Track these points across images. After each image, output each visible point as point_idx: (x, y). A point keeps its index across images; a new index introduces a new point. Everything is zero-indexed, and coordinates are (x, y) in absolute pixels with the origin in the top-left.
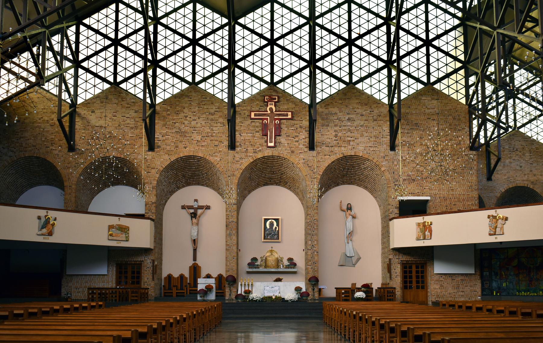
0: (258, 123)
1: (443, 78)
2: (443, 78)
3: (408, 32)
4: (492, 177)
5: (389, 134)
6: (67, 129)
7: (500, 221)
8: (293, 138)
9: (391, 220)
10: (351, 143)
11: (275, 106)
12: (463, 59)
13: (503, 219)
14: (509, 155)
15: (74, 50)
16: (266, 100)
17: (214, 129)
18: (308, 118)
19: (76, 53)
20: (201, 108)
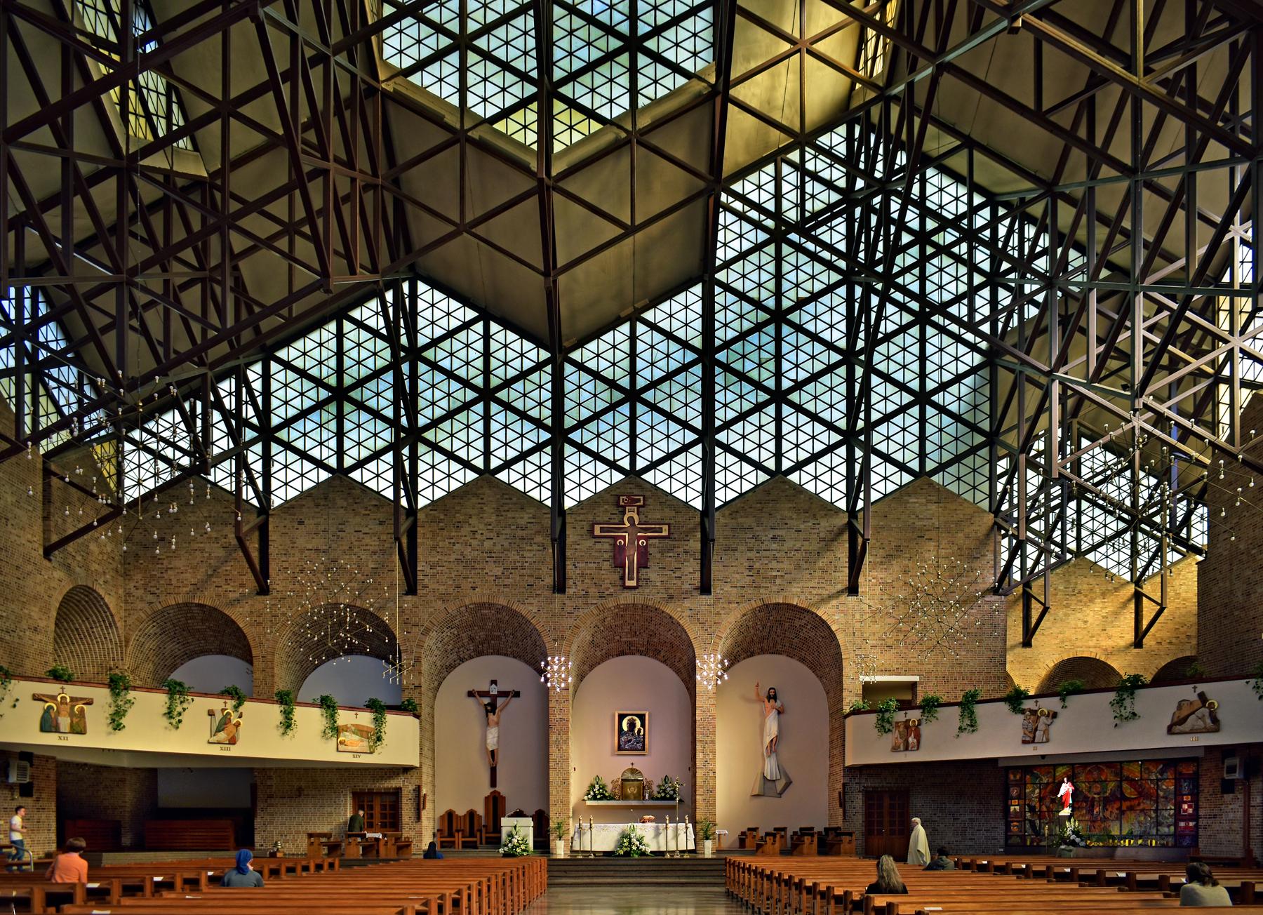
10: (778, 581)
11: (638, 514)
13: (1048, 716)
16: (622, 503)
17: (526, 554)
19: (264, 413)
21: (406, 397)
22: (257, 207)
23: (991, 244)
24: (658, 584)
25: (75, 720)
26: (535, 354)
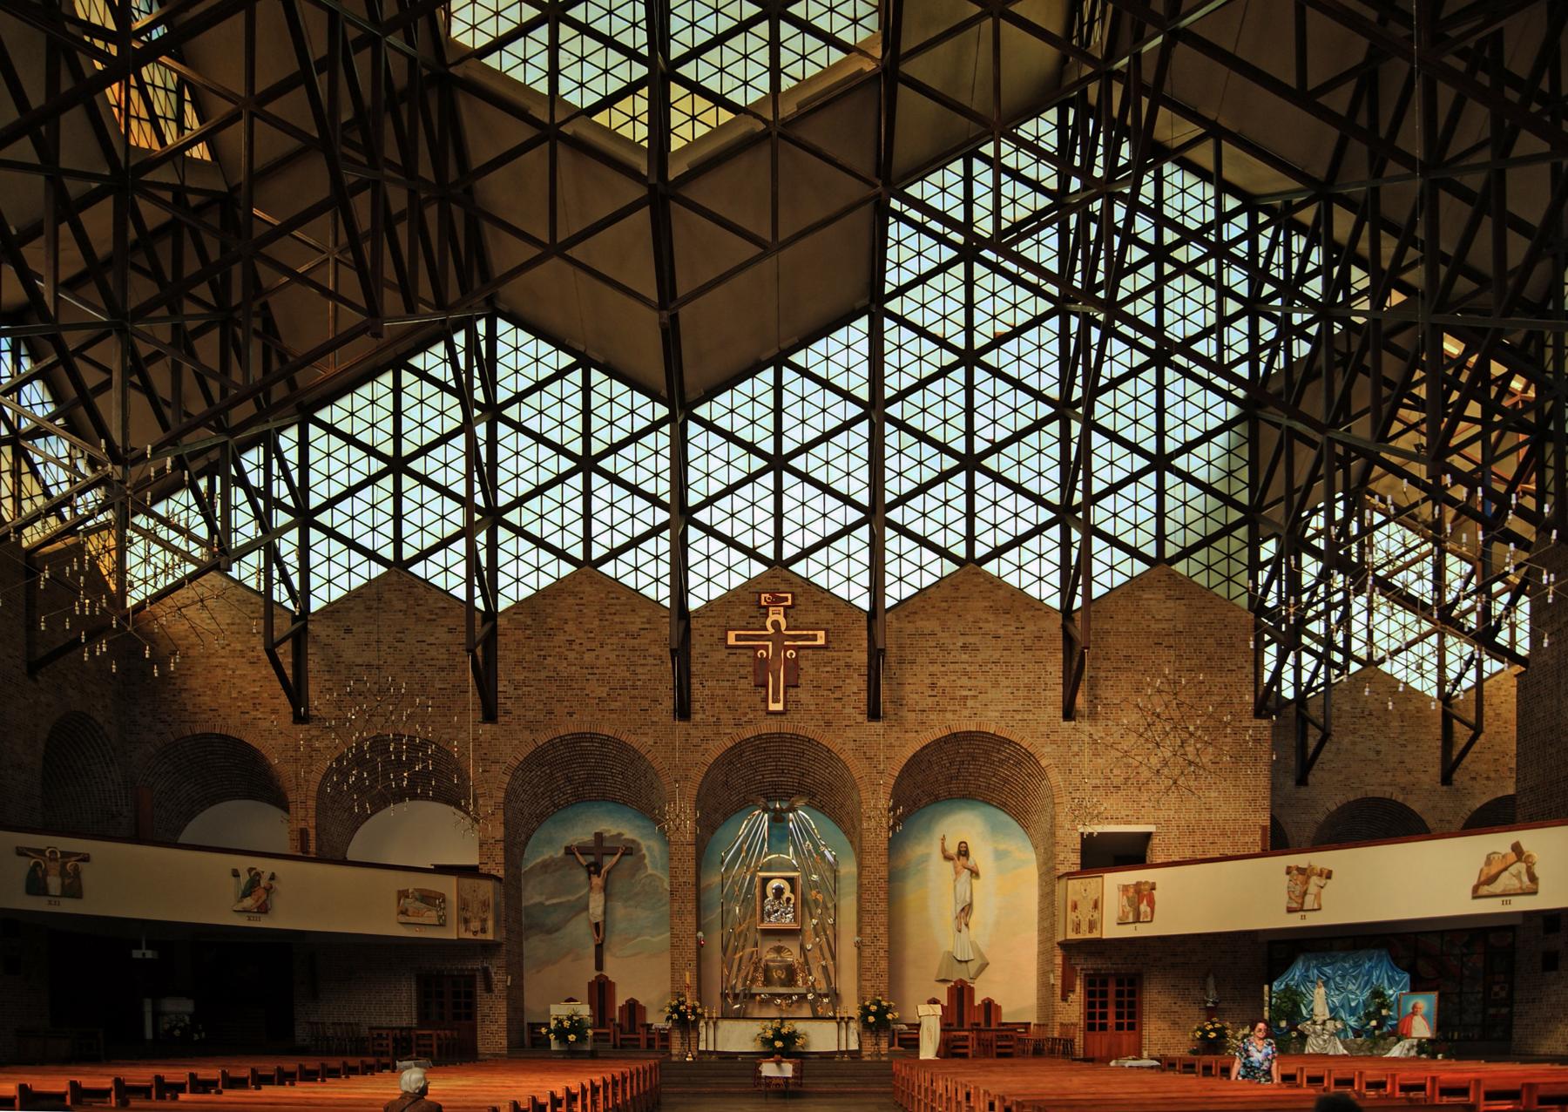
6: (289, 672)
10: (970, 703)
11: (785, 616)
16: (763, 603)
18: (865, 644)
19: (301, 491)
21: (483, 469)
25: (67, 881)
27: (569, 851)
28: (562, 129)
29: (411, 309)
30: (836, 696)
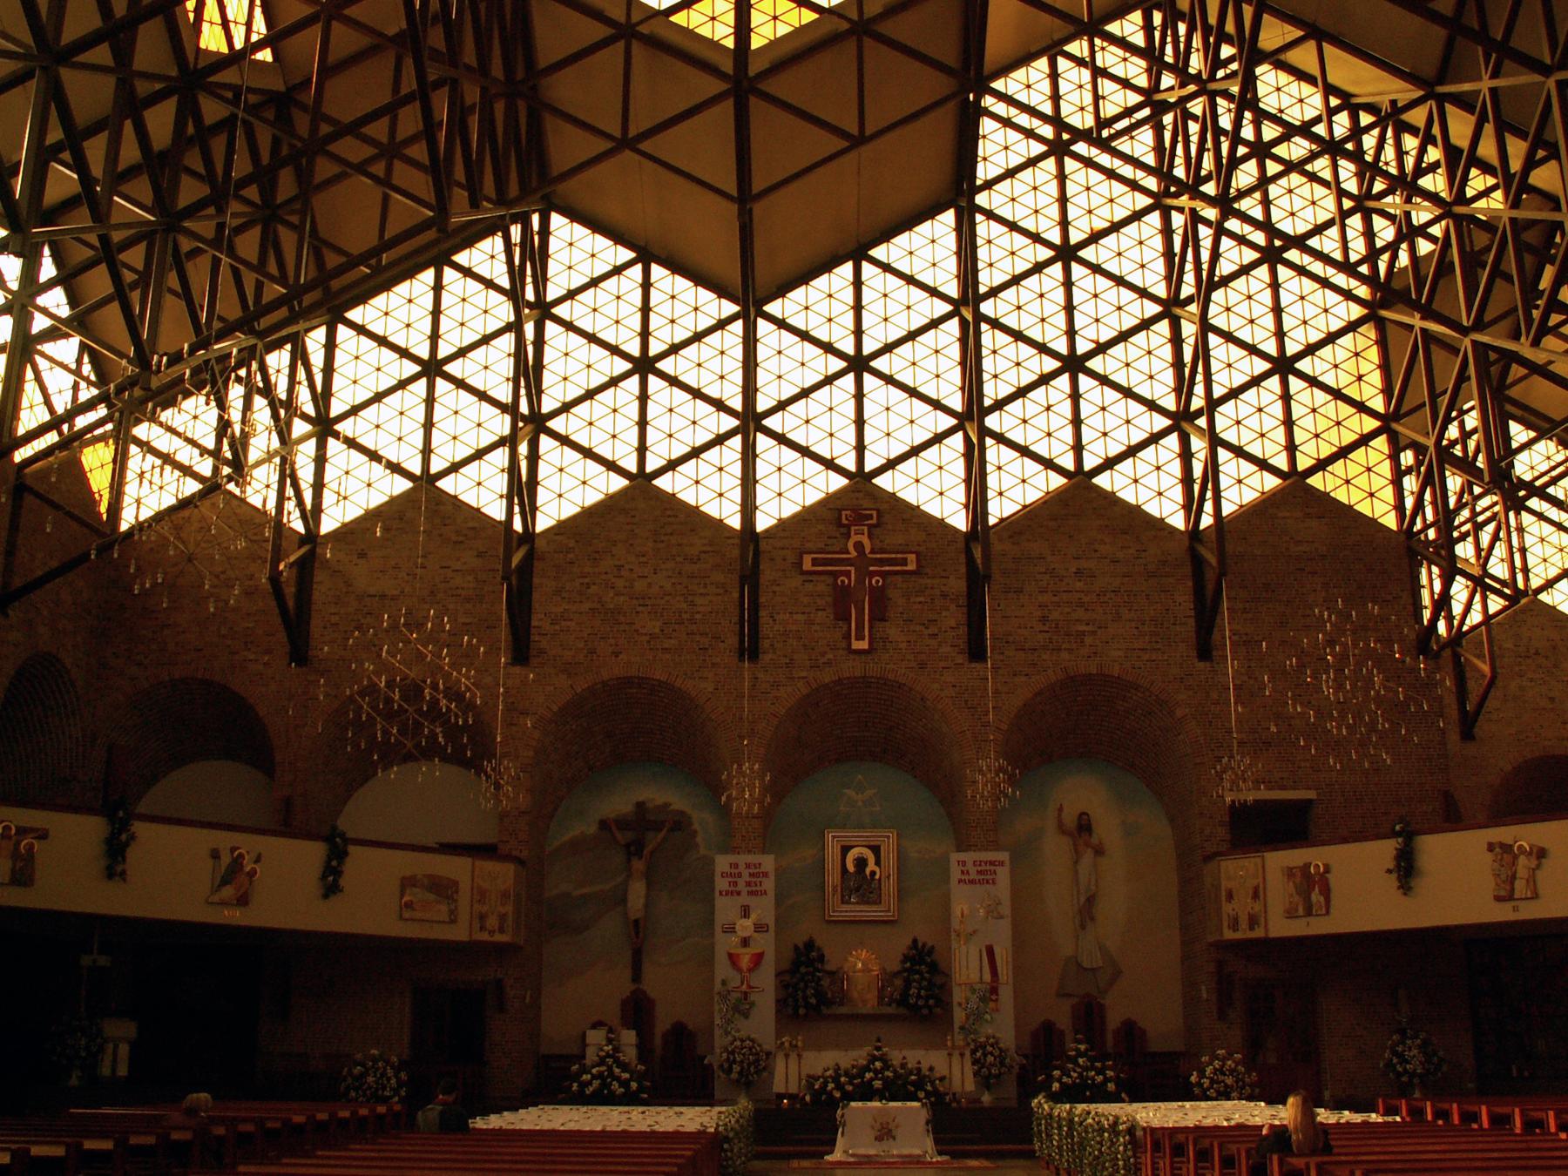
0: (822, 586)
1: (1332, 459)
2: (1332, 459)
3: (1229, 337)
4: (1476, 730)
5: (1192, 613)
6: (291, 604)
7: (1522, 860)
8: (922, 628)
9: (1208, 858)
10: (1088, 640)
11: (870, 537)
12: (1381, 408)
13: (1530, 853)
14: (1517, 669)
15: (319, 389)
16: (844, 521)
17: (699, 601)
18: (963, 569)
19: (323, 398)
20: (662, 545)
21: (528, 372)
22: (353, 129)
23: (1357, 156)
24: (903, 646)
25: (20, 864)
26: (717, 307)
27: (604, 824)
28: (637, 28)
29: (475, 204)
30: (930, 631)
